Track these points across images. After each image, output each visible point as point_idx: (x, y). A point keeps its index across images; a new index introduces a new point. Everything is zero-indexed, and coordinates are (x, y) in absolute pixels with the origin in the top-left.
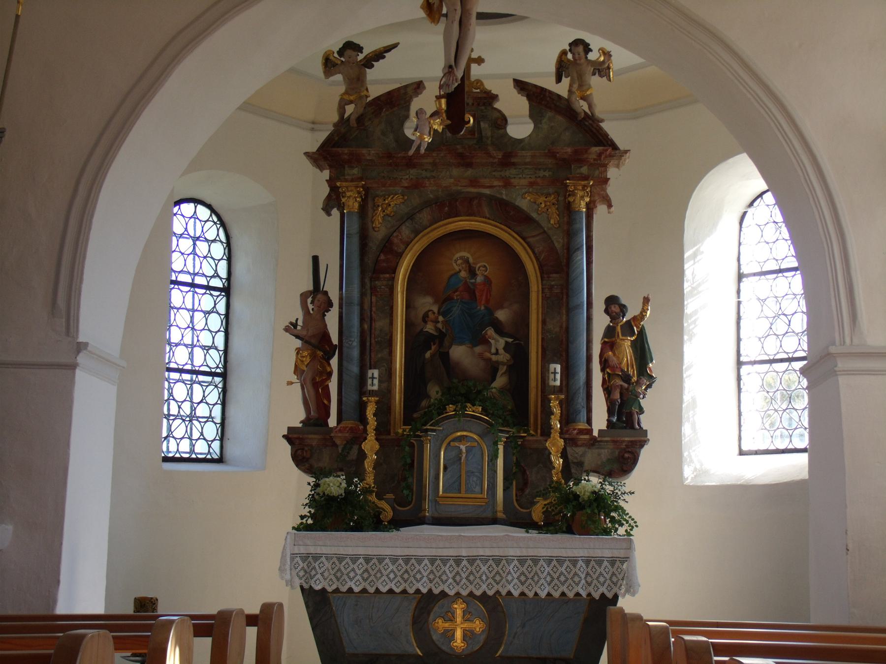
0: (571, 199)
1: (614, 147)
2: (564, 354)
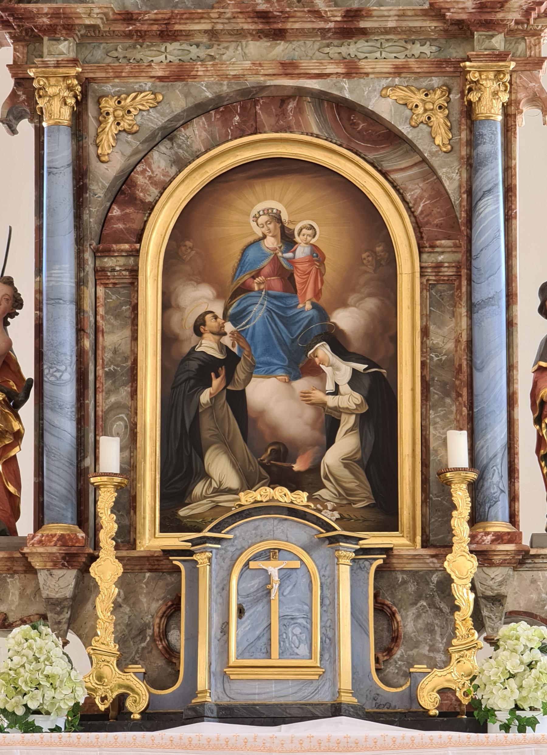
0: (473, 97)
2: (465, 392)
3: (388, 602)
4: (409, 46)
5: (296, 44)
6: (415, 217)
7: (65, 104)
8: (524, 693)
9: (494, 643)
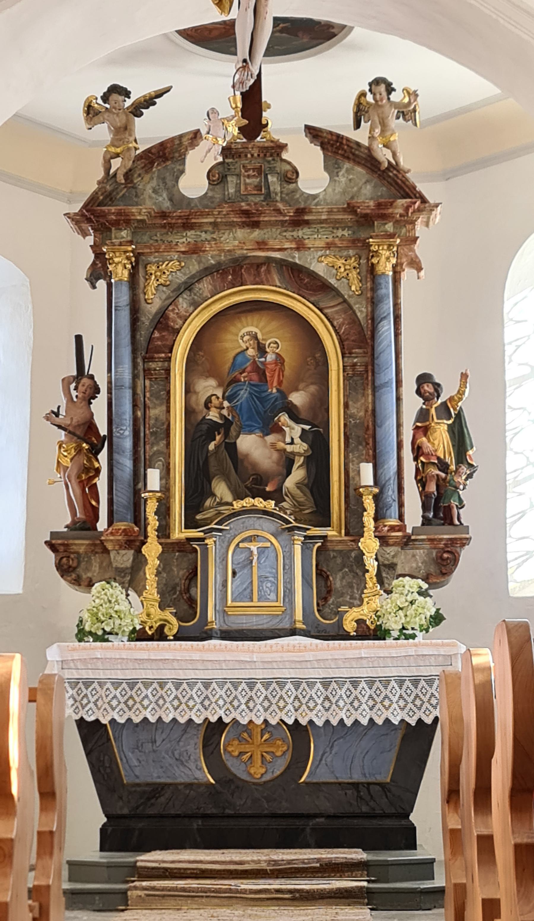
0: (375, 261)
1: (424, 201)
2: (371, 441)
3: (325, 569)
4: (335, 231)
5: (265, 231)
6: (340, 336)
7: (125, 268)
8: (408, 619)
9: (389, 592)
